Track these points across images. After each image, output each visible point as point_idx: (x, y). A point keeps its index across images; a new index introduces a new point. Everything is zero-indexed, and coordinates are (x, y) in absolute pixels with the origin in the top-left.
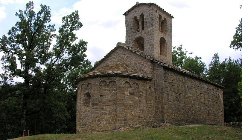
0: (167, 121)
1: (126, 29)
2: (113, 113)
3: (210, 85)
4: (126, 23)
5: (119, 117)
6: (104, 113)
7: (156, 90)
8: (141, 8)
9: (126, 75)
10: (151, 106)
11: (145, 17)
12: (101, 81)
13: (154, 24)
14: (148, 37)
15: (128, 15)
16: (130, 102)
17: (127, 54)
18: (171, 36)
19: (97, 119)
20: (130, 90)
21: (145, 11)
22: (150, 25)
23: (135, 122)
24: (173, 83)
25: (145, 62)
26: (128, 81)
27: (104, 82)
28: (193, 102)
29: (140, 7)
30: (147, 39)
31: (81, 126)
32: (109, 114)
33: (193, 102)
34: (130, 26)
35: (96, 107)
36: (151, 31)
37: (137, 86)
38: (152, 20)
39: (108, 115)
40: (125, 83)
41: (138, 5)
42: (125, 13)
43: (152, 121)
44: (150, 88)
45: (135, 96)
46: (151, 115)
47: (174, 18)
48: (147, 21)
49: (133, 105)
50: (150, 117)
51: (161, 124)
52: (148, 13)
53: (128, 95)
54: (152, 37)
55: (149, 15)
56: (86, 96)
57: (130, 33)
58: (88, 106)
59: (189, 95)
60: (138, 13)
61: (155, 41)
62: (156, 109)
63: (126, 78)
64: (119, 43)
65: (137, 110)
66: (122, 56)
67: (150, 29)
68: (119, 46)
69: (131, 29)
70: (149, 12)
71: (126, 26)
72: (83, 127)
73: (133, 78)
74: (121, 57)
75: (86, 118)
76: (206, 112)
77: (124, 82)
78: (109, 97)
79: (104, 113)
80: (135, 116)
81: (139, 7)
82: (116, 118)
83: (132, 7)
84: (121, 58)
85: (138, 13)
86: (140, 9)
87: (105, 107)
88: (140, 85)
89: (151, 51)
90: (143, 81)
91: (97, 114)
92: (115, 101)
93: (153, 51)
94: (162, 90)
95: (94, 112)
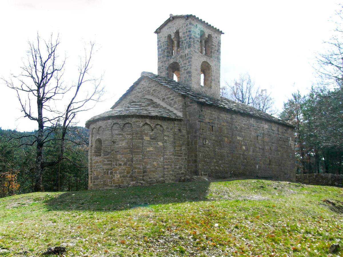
0: (203, 173)
1: (159, 51)
2: (128, 163)
3: (273, 125)
4: (158, 44)
5: (135, 168)
6: (118, 164)
7: (188, 133)
8: (176, 22)
9: (144, 115)
10: (182, 153)
11: (181, 35)
12: (114, 124)
13: (192, 43)
14: (185, 62)
15: (160, 32)
16: (151, 149)
17: (154, 86)
18: (218, 59)
19: (110, 171)
20: (151, 134)
21: (181, 26)
22: (187, 46)
23: (158, 174)
24: (212, 123)
25: (174, 96)
26: (149, 123)
27: (116, 124)
28: (244, 148)
29: (174, 21)
30: (183, 65)
31: (93, 181)
32: (124, 165)
33: (244, 148)
34: (163, 48)
35: (107, 156)
36: (188, 54)
37: (162, 129)
38: (190, 38)
39: (122, 166)
40: (144, 125)
41: (173, 19)
42: (157, 30)
43: (182, 173)
44: (180, 130)
45: (158, 142)
46: (181, 166)
47: (223, 33)
48: (183, 41)
49: (156, 153)
50: (180, 168)
51: (193, 177)
52: (185, 29)
53: (148, 140)
54: (189, 62)
55: (185, 32)
56: (98, 143)
57: (163, 57)
58: (100, 156)
59: (238, 138)
60: (172, 30)
61: (193, 67)
62: (188, 158)
63: (145, 118)
64: (143, 73)
65: (160, 159)
66: (148, 89)
67: (186, 52)
68: (146, 77)
69: (164, 51)
70: (186, 27)
71: (158, 49)
72: (95, 182)
73: (154, 119)
74: (147, 91)
75: (97, 170)
76: (265, 160)
77: (142, 123)
78: (124, 144)
79: (118, 164)
80: (158, 167)
81: (174, 21)
82: (132, 170)
83: (165, 22)
84: (146, 92)
85: (172, 30)
86: (174, 24)
87: (119, 156)
88: (165, 127)
89: (188, 81)
90: (169, 122)
91: (110, 165)
92: (131, 148)
93: (191, 80)
94: (196, 133)
95: (106, 162)
